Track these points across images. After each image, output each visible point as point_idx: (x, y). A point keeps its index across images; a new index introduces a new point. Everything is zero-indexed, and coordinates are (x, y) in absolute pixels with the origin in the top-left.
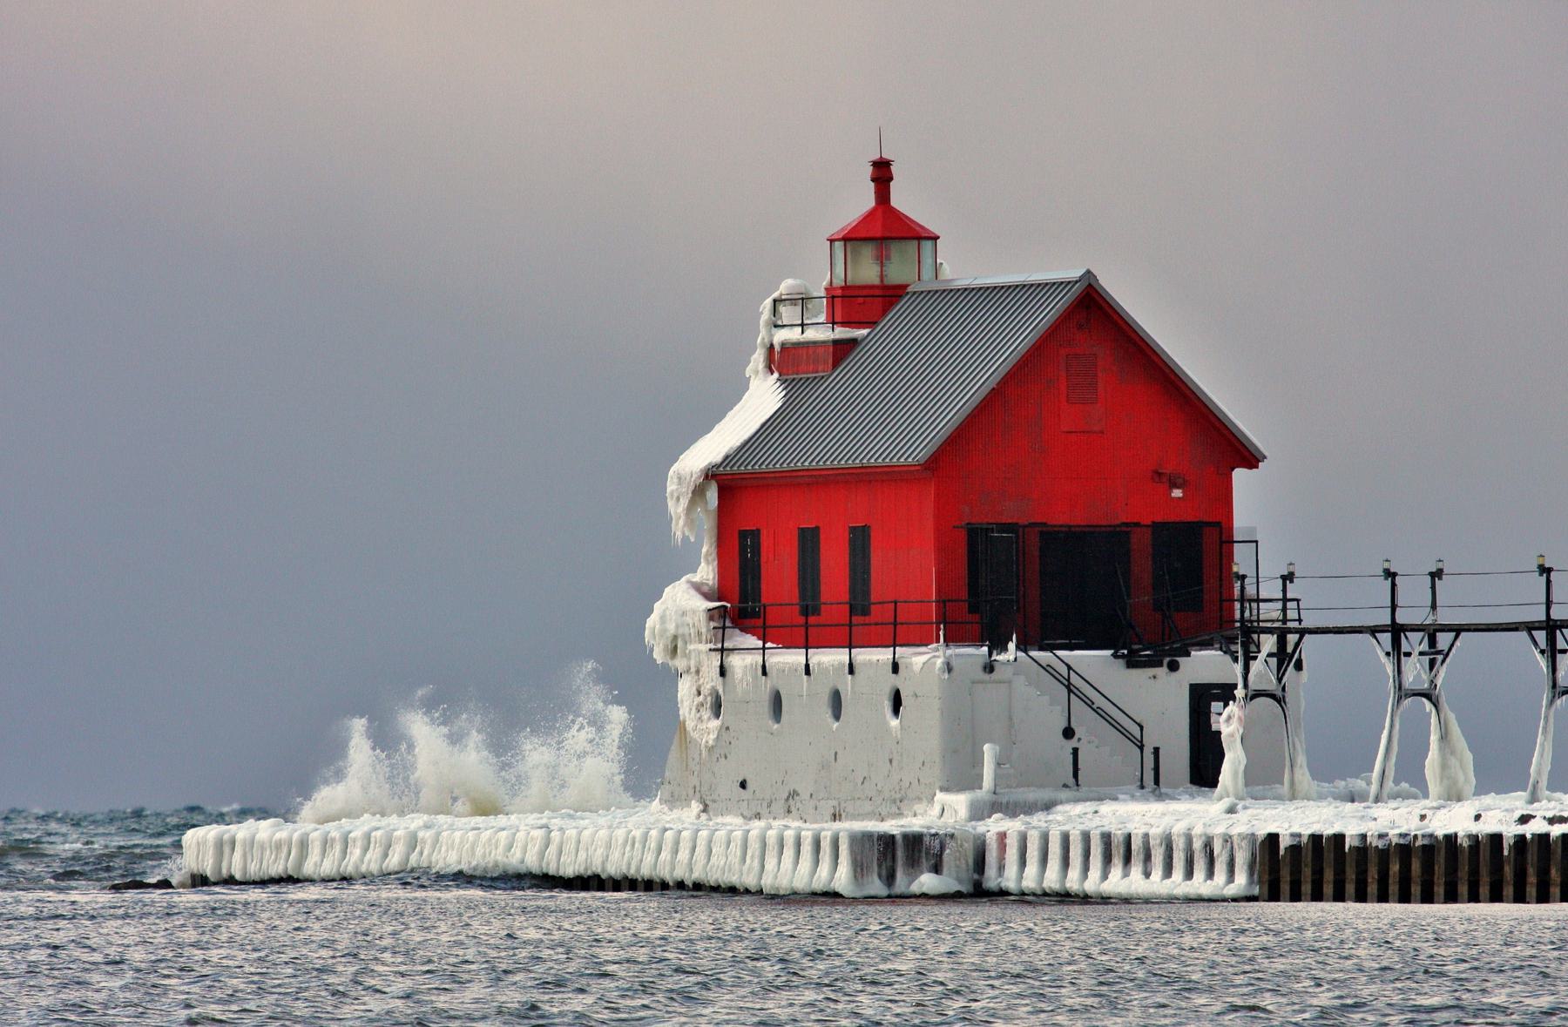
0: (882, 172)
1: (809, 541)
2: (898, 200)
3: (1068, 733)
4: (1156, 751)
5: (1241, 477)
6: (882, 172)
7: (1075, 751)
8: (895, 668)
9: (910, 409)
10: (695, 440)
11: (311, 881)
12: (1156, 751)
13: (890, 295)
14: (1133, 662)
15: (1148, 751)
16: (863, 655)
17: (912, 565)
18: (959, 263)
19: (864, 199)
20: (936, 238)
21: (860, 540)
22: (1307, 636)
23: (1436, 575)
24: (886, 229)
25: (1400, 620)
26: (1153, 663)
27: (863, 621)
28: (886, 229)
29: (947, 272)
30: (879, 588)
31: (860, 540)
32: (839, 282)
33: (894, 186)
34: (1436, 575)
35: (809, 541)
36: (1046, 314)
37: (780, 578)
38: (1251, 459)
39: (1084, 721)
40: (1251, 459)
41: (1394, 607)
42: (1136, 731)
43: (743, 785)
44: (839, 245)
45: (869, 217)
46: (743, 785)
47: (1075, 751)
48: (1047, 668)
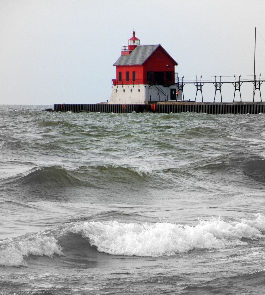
0: (134, 33)
1: (128, 73)
2: (136, 36)
3: (158, 94)
4: (168, 96)
5: (175, 67)
6: (134, 33)
7: (159, 96)
8: (139, 87)
9: (139, 59)
10: (119, 59)
11: (50, 212)
12: (168, 96)
13: (135, 46)
14: (165, 86)
15: (167, 96)
16: (135, 85)
17: (140, 75)
18: (143, 43)
19: (132, 36)
20: (140, 40)
21: (134, 73)
22: (205, 84)
23: (221, 77)
24: (134, 39)
25: (197, 82)
26: (167, 86)
27: (134, 81)
28: (134, 39)
29: (140, 44)
30: (136, 78)
31: (134, 73)
32: (130, 45)
33: (135, 34)
34: (201, 77)
35: (128, 73)
36: (156, 47)
37: (124, 77)
38: (177, 64)
39: (160, 93)
40: (177, 64)
41: (260, 79)
42: (165, 94)
43: (120, 99)
44: (129, 41)
45: (133, 38)
46: (120, 99)
47: (159, 96)
48: (156, 87)
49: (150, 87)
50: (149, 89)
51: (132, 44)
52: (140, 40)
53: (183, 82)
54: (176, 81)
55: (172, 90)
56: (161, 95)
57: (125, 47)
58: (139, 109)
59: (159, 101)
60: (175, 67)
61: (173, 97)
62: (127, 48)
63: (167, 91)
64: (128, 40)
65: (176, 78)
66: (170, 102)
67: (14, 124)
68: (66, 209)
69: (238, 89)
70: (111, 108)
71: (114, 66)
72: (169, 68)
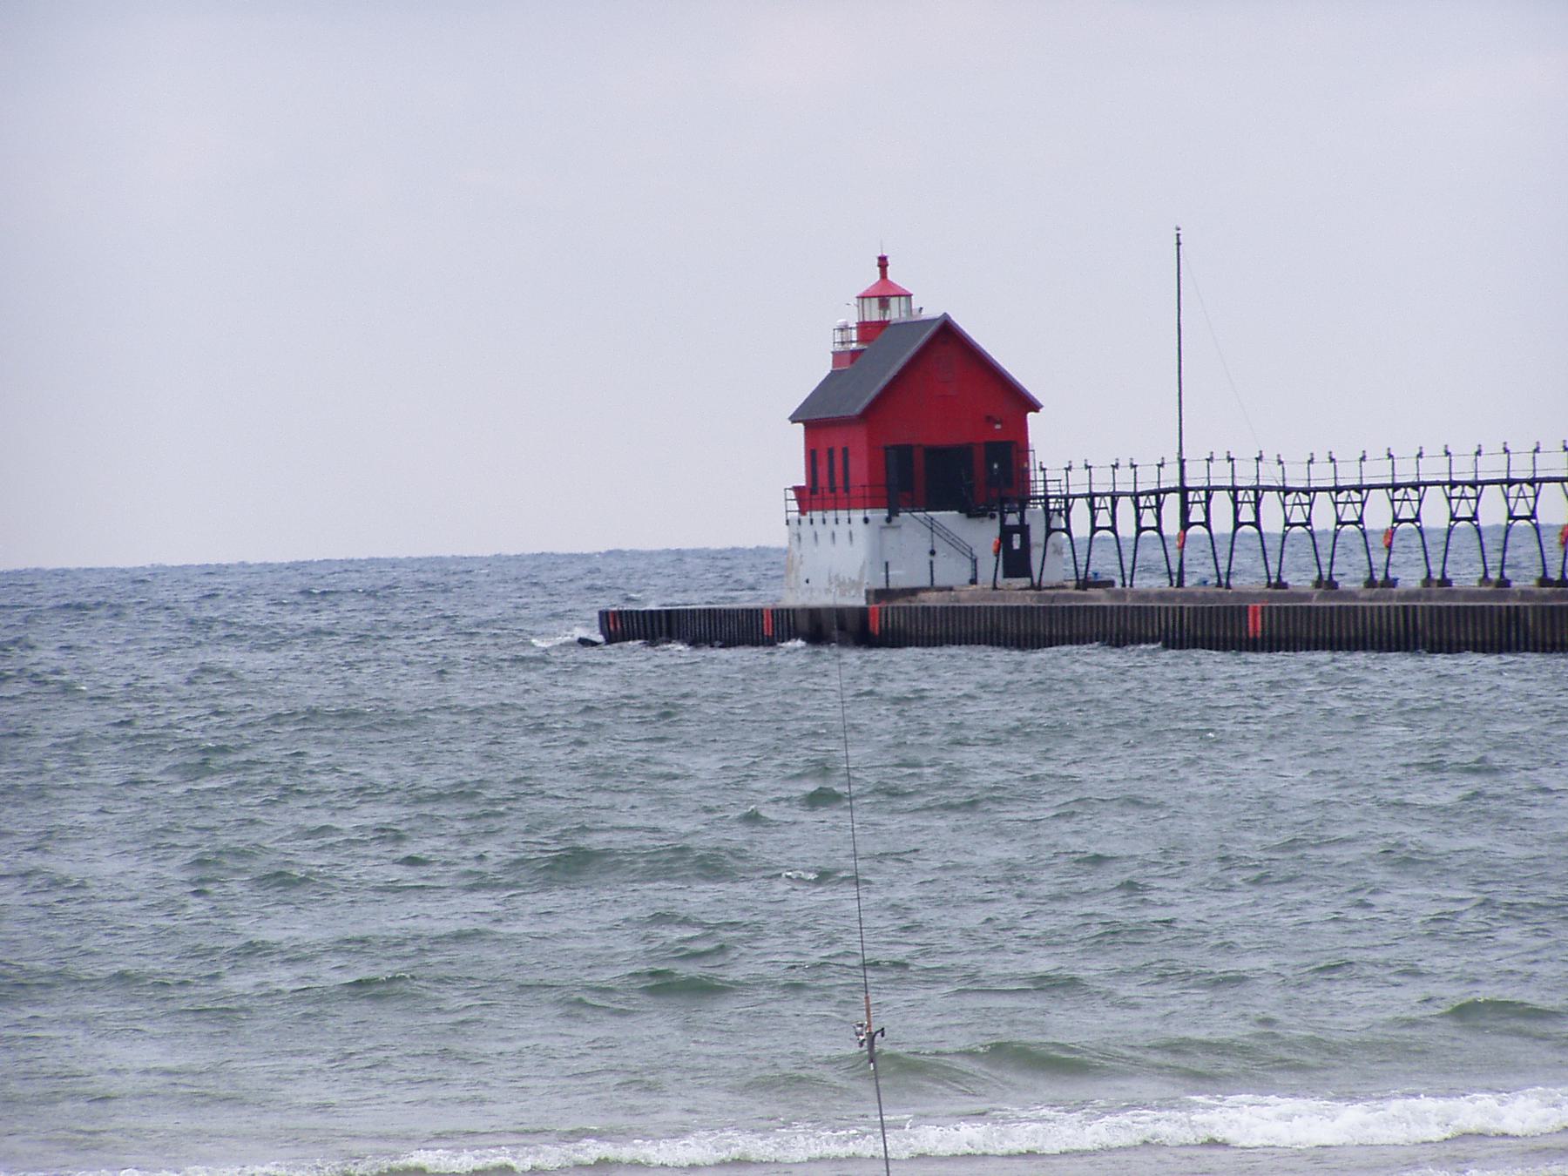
0: (883, 262)
5: (1030, 415)
6: (883, 262)
20: (909, 296)
24: (884, 293)
28: (884, 293)
36: (937, 324)
38: (1035, 407)
40: (1035, 407)
49: (889, 520)
50: (890, 536)
51: (874, 315)
52: (909, 296)
53: (1238, 484)
54: (1039, 489)
55: (1006, 533)
56: (942, 553)
57: (844, 329)
58: (820, 628)
59: (932, 588)
60: (1030, 415)
61: (1016, 562)
62: (854, 335)
63: (983, 535)
64: (862, 297)
65: (1036, 475)
66: (1016, 593)
67: (131, 680)
68: (428, 1086)
69: (1109, 524)
70: (1483, 627)
71: (794, 419)
72: (998, 427)
